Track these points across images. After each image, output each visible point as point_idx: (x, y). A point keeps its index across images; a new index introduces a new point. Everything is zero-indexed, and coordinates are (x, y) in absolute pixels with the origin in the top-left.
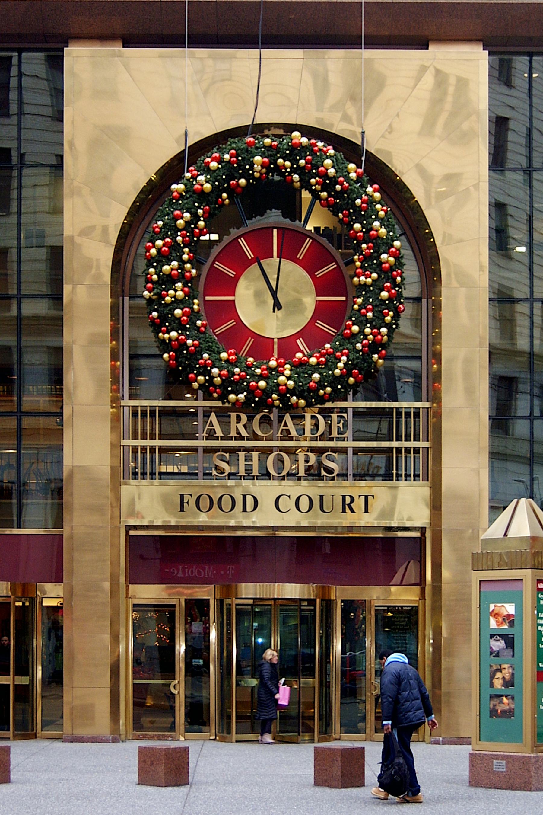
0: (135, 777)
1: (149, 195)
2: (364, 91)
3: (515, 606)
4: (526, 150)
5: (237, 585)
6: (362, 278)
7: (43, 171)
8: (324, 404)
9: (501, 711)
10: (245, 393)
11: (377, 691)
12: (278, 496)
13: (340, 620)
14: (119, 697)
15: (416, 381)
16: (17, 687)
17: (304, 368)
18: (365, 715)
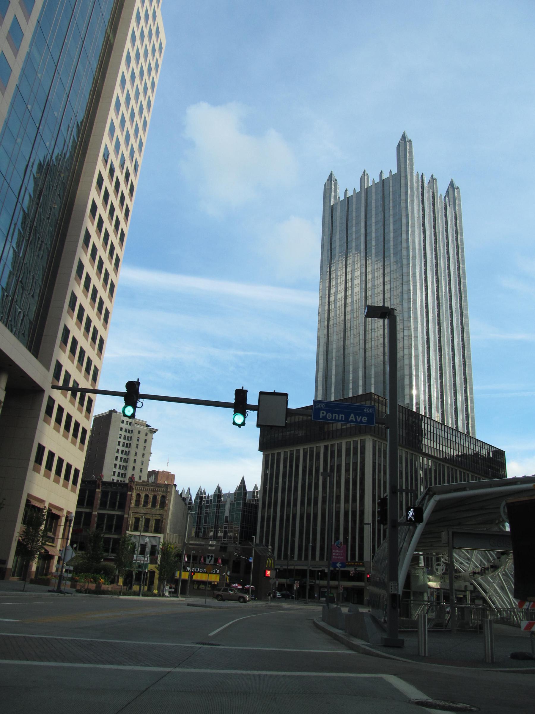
0: (249, 394)
1: (27, 566)
2: (89, 662)
3: (246, 400)
4: (460, 379)
5: (456, 590)
6: (57, 547)
7: (338, 233)
8: (321, 475)
9: (279, 584)
10: (412, 510)
11: (402, 518)
12: (21, 186)
13: (32, 452)
14: (17, 518)
15: (428, 580)
16: (86, 513)
17: (351, 255)
18: (445, 460)
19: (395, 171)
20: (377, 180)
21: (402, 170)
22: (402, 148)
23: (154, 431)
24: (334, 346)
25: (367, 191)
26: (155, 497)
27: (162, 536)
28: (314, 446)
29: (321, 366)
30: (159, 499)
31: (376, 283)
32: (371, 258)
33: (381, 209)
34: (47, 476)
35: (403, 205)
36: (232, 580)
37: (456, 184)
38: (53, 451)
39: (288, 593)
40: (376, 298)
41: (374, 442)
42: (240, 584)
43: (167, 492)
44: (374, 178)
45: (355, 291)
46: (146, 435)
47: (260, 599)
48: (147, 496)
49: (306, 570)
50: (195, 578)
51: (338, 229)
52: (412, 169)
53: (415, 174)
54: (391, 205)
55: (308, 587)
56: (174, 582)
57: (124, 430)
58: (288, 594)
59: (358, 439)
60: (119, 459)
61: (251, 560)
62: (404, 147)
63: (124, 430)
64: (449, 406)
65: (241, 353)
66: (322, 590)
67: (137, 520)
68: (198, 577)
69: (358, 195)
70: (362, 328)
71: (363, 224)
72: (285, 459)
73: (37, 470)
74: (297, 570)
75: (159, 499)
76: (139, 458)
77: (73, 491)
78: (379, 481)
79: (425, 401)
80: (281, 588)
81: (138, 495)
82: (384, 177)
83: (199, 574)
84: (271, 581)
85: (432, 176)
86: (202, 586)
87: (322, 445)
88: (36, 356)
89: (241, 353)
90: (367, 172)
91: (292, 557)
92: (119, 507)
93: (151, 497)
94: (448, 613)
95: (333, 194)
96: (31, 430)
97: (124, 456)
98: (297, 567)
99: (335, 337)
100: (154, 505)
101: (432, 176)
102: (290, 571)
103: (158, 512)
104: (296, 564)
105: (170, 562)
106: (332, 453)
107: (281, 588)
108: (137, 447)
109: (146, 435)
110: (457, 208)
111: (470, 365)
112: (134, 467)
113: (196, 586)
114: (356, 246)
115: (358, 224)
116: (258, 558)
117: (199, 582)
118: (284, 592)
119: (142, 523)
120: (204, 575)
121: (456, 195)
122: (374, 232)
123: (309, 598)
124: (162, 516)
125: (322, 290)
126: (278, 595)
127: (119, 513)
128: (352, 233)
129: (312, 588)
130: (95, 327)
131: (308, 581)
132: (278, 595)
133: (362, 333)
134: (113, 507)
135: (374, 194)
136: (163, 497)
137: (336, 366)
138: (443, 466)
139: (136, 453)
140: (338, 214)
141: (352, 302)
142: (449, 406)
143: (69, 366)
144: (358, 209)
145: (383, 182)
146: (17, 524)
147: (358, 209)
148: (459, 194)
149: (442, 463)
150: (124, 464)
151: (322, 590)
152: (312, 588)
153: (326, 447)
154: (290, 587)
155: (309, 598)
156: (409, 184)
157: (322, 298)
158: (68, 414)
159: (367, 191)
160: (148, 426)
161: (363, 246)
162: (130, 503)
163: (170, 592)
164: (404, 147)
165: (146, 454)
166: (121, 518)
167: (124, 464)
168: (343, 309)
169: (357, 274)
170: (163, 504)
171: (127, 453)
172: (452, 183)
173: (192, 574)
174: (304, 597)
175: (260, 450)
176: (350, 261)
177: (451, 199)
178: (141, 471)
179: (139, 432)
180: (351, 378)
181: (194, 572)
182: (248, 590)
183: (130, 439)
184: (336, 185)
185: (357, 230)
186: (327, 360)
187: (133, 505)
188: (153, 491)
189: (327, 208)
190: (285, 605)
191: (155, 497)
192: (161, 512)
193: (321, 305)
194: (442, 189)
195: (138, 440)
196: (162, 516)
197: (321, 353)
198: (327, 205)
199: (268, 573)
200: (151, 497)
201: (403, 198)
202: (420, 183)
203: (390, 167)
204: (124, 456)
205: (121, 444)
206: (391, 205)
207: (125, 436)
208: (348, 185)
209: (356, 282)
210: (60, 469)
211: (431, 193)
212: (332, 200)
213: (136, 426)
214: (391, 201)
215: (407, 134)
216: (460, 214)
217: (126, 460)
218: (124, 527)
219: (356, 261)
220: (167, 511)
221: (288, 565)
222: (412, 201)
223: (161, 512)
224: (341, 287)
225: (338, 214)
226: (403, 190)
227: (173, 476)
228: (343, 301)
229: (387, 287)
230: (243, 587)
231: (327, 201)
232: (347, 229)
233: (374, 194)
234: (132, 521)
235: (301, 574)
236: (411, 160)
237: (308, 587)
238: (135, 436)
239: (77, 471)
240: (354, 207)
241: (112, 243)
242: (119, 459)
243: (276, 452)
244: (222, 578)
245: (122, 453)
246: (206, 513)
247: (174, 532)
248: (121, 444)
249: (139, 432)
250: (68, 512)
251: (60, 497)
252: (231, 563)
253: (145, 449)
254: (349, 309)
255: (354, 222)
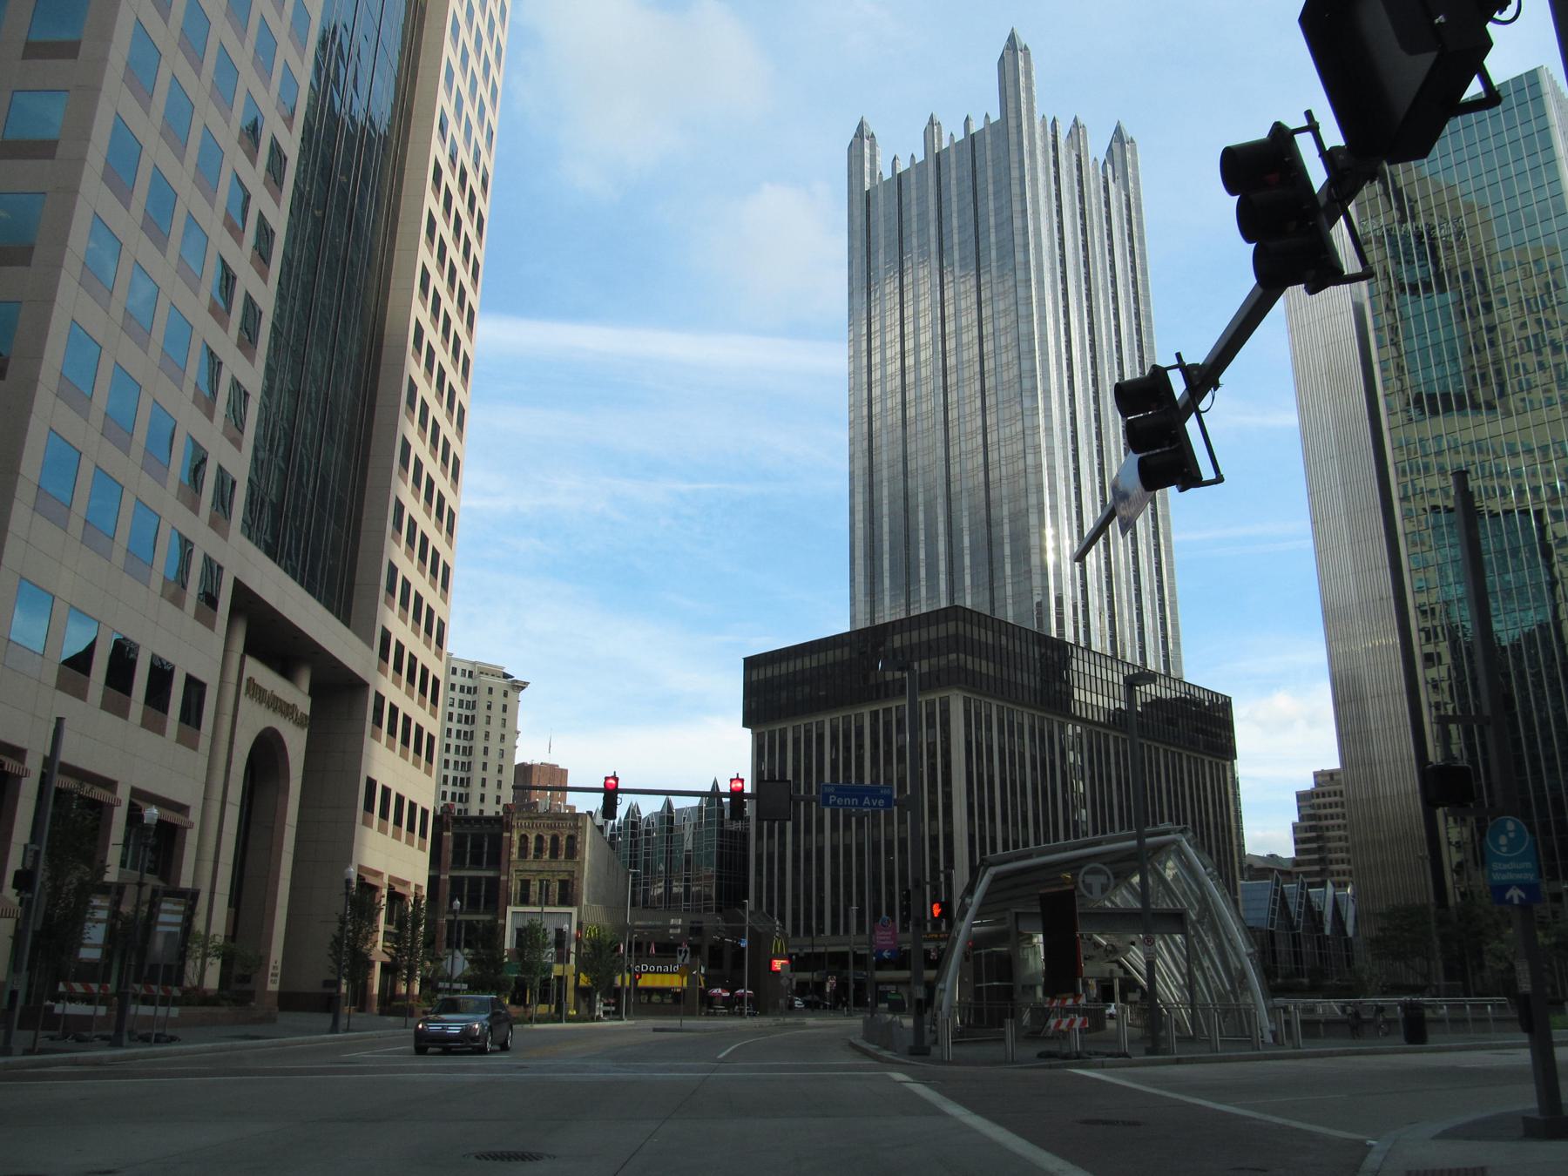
19: (995, 116)
20: (959, 136)
21: (1012, 115)
22: (1009, 68)
23: (520, 686)
24: (885, 492)
25: (939, 159)
26: (555, 839)
27: (574, 910)
28: (852, 713)
29: (859, 499)
30: (563, 842)
31: (965, 357)
32: (952, 272)
33: (970, 197)
34: (382, 830)
35: (1016, 189)
36: (711, 982)
37: (1128, 132)
38: (389, 785)
39: (816, 998)
40: (967, 390)
41: (967, 702)
42: (725, 988)
43: (576, 827)
44: (952, 131)
45: (923, 357)
46: (506, 694)
47: (764, 1013)
48: (539, 838)
49: (845, 954)
50: (640, 983)
51: (882, 242)
52: (1031, 110)
53: (1037, 121)
54: (991, 188)
55: (852, 986)
56: (615, 994)
57: (457, 688)
58: (815, 999)
59: (935, 697)
60: (453, 749)
61: (744, 944)
62: (1012, 58)
63: (457, 688)
64: (1125, 604)
65: (684, 487)
66: (881, 988)
67: (526, 884)
68: (647, 981)
69: (919, 168)
70: (940, 434)
71: (933, 231)
72: (796, 742)
73: (367, 823)
74: (832, 954)
75: (563, 842)
76: (494, 746)
77: (422, 848)
78: (980, 776)
79: (1074, 597)
80: (802, 989)
81: (524, 838)
82: (975, 127)
83: (649, 976)
84: (784, 982)
85: (1075, 120)
86: (656, 998)
87: (866, 711)
88: (348, 626)
89: (684, 487)
90: (937, 118)
91: (821, 930)
92: (489, 863)
93: (548, 839)
94: (1111, 1016)
95: (867, 165)
96: (356, 755)
97: (462, 743)
98: (831, 949)
99: (884, 437)
100: (554, 854)
101: (1075, 120)
102: (819, 956)
103: (563, 867)
104: (827, 943)
105: (599, 957)
106: (887, 725)
107: (802, 989)
108: (488, 722)
109: (506, 694)
110: (1131, 185)
111: (1166, 518)
112: (485, 765)
113: (644, 999)
114: (919, 246)
115: (923, 230)
116: (756, 938)
117: (650, 991)
118: (809, 998)
119: (535, 887)
120: (658, 976)
121: (1128, 156)
122: (956, 247)
123: (856, 1004)
124: (571, 873)
125: (854, 342)
126: (798, 1003)
127: (491, 874)
128: (910, 219)
129: (860, 986)
130: (411, 518)
131: (851, 973)
132: (798, 1003)
133: (940, 427)
134: (477, 862)
135: (953, 166)
136: (572, 839)
137: (891, 532)
138: (1106, 736)
139: (487, 735)
140: (881, 210)
141: (918, 380)
142: (1125, 604)
143: (401, 630)
144: (922, 200)
145: (972, 140)
146: (21, 800)
147: (922, 200)
148: (1134, 154)
149: (1102, 731)
150: (465, 759)
151: (881, 988)
152: (860, 986)
153: (875, 715)
154: (820, 987)
155: (856, 1004)
156: (1026, 142)
157: (854, 358)
158: (392, 705)
159: (939, 159)
160: (506, 676)
161: (934, 247)
162: (510, 853)
163: (605, 1013)
164: (1012, 58)
165: (508, 735)
166: (494, 883)
167: (465, 759)
168: (899, 413)
169: (924, 304)
170: (572, 851)
171: (469, 736)
172: (1118, 131)
173: (636, 976)
174: (845, 1004)
175: (745, 725)
176: (907, 280)
177: (1118, 166)
178: (500, 771)
179: (490, 690)
180: (922, 556)
181: (640, 974)
182: (741, 997)
183: (472, 705)
184: (873, 147)
185: (924, 234)
186: (871, 487)
187: (515, 856)
188: (550, 827)
189: (857, 198)
190: (810, 1021)
191: (555, 839)
192: (569, 866)
193: (854, 374)
194: (1096, 148)
195: (489, 707)
196: (571, 873)
197: (859, 508)
198: (857, 190)
199: (778, 964)
200: (548, 839)
201: (1015, 173)
202: (1050, 139)
203: (985, 107)
204: (462, 743)
205: (455, 718)
206: (991, 188)
207: (461, 701)
208: (899, 148)
209: (924, 372)
210: (399, 812)
211: (1074, 159)
212: (867, 179)
213: (483, 677)
214: (990, 181)
215: (1018, 32)
216: (1138, 198)
217: (468, 751)
218: (502, 900)
219: (922, 277)
220: (580, 864)
221: (813, 946)
222: (1034, 180)
223: (569, 866)
224: (893, 351)
225: (881, 208)
226: (1014, 157)
227: (564, 773)
228: (899, 396)
229: (988, 346)
230: (732, 993)
231: (855, 182)
232: (901, 242)
233: (953, 166)
234: (515, 887)
235: (839, 960)
236: (1029, 89)
237: (852, 986)
238: (482, 699)
239: (425, 812)
240: (914, 194)
241: (417, 322)
242: (453, 749)
243: (777, 727)
244: (693, 980)
245: (458, 736)
246: (647, 854)
247: (595, 902)
248: (455, 718)
249: (490, 690)
250: (418, 887)
251: (396, 860)
252: (706, 951)
253: (504, 725)
254: (910, 395)
255: (915, 226)
